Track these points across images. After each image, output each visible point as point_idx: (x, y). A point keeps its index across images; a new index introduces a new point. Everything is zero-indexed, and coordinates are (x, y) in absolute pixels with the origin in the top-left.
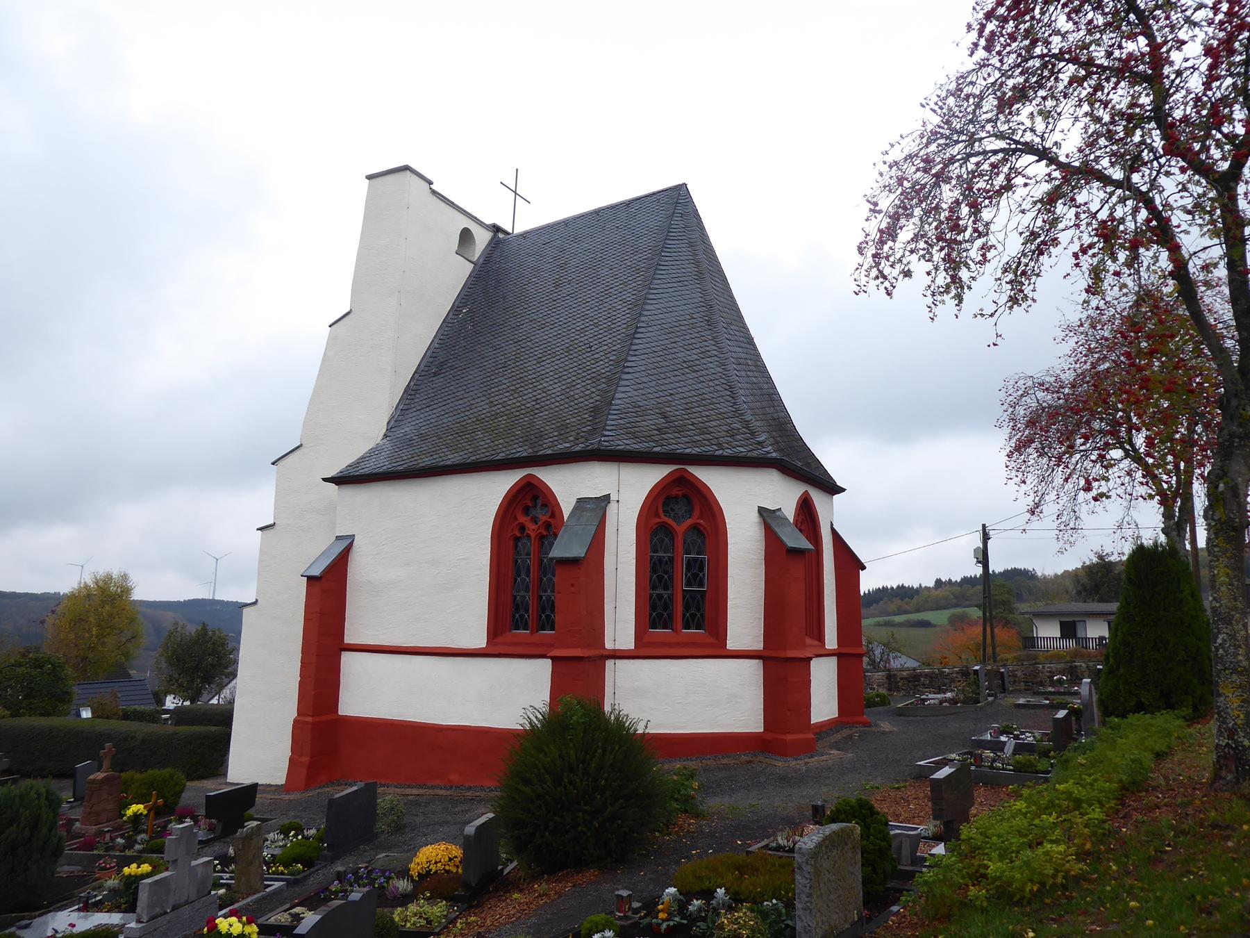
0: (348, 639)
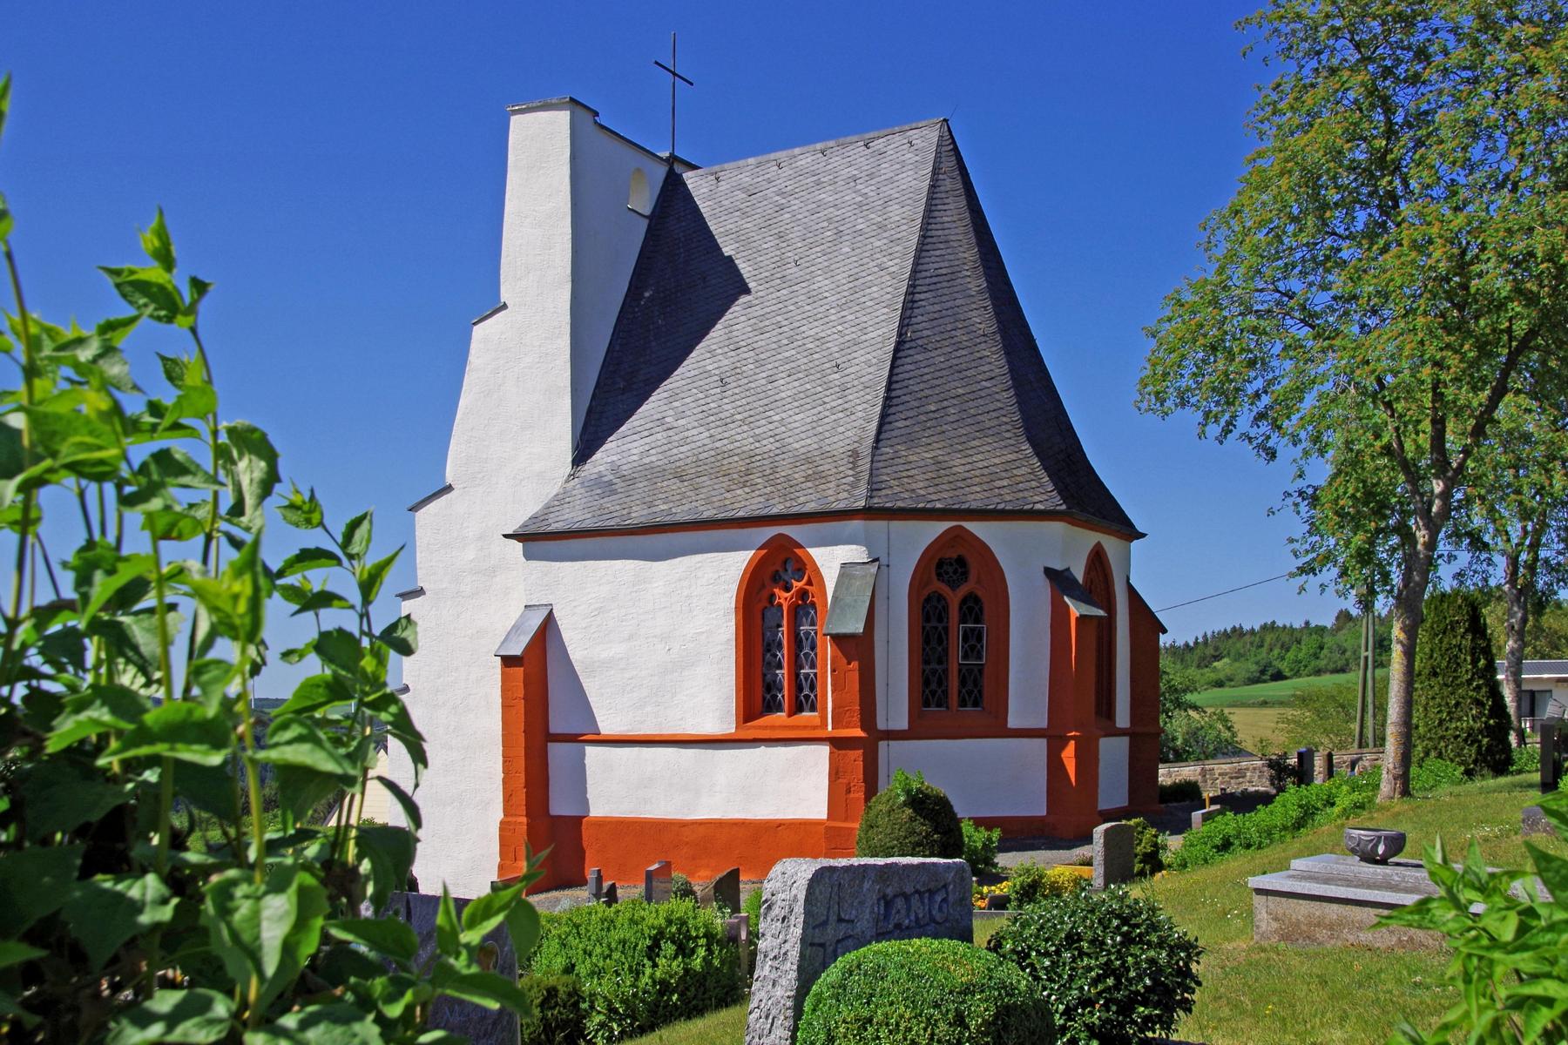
0: (555, 728)
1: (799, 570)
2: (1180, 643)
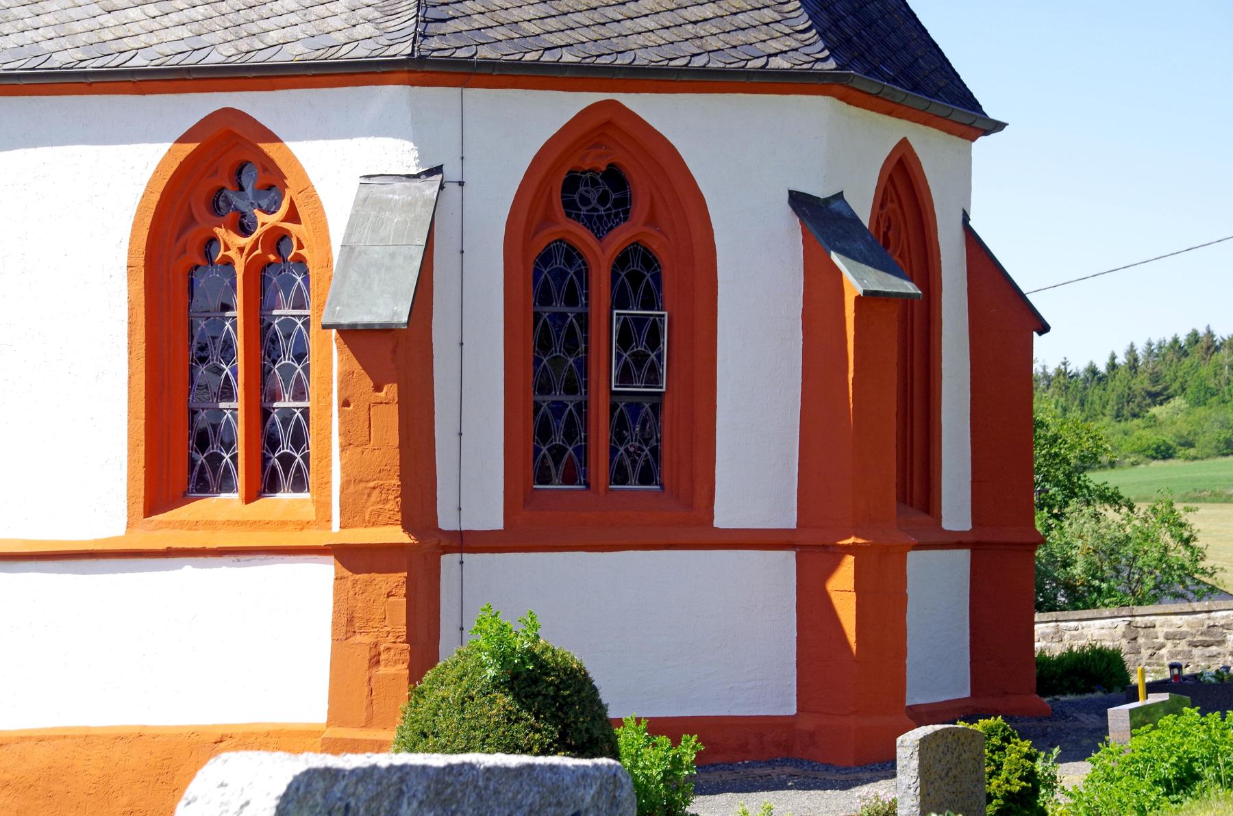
1: (270, 188)
2: (1078, 365)
